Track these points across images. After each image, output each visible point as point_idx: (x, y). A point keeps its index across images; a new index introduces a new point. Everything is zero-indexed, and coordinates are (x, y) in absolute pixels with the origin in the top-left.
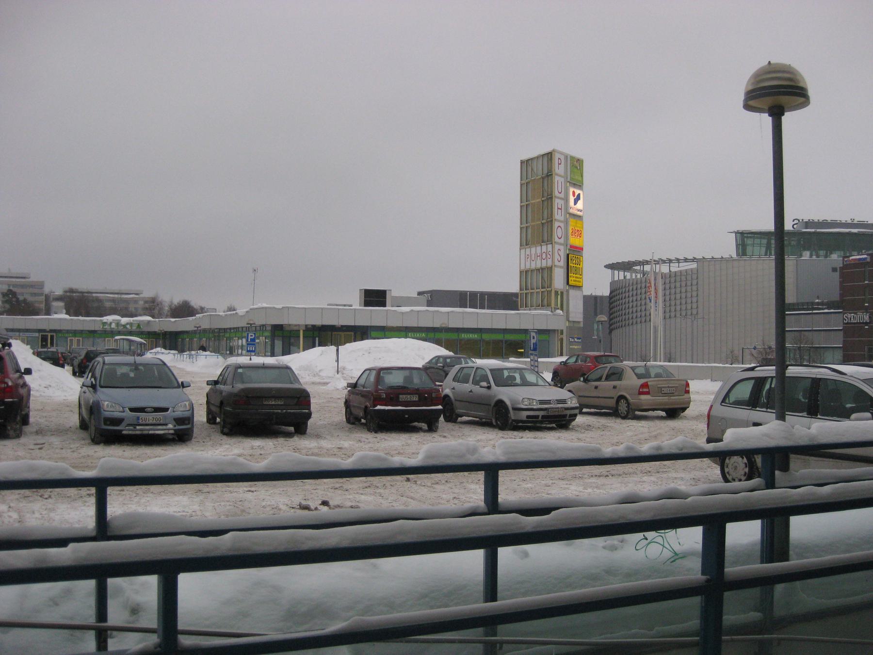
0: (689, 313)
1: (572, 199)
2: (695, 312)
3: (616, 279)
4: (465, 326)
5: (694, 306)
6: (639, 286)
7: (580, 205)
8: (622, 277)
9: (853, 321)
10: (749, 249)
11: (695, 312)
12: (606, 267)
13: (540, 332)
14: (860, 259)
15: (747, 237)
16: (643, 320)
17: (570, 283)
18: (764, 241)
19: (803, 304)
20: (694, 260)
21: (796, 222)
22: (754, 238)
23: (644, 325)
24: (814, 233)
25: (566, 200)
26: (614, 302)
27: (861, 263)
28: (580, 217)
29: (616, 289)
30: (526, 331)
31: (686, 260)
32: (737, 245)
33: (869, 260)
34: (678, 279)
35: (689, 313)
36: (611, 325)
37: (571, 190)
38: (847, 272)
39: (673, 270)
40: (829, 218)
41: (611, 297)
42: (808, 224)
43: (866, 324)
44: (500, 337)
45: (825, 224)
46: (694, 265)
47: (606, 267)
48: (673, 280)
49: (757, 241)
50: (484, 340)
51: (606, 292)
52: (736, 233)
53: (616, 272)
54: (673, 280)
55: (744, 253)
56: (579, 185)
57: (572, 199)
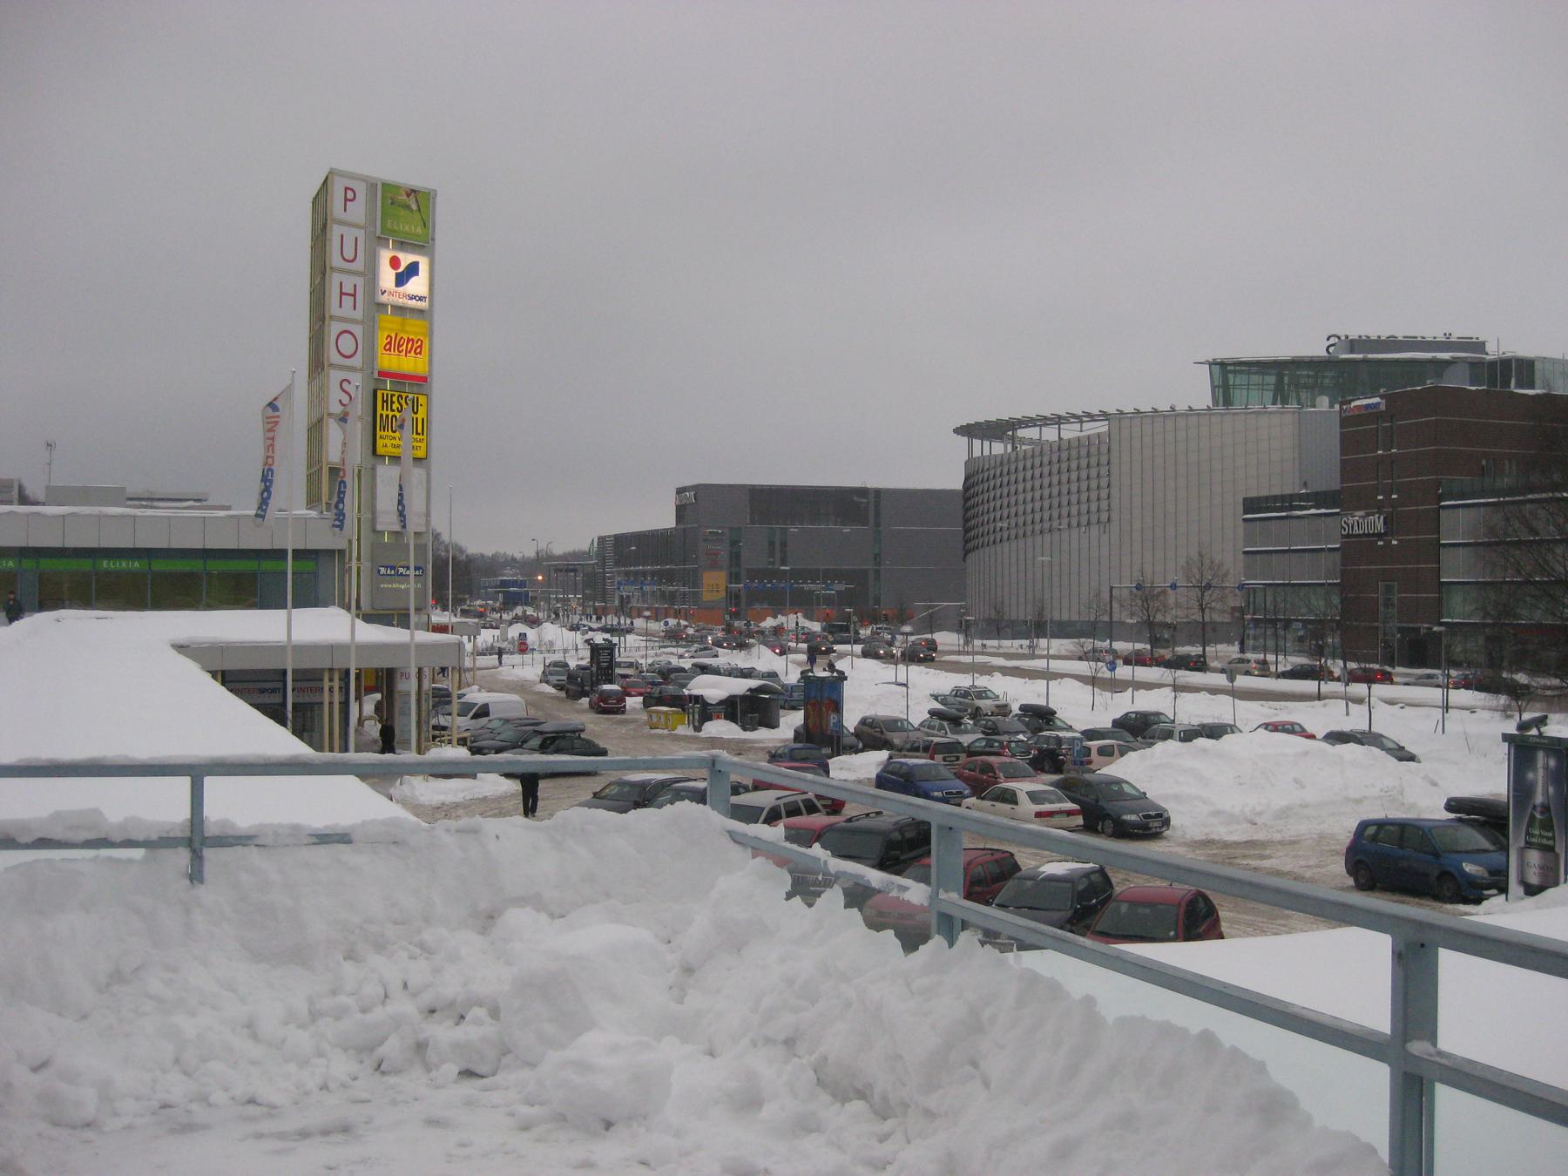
0: (1094, 519)
1: (387, 277)
2: (1104, 517)
3: (977, 453)
4: (176, 545)
5: (1104, 505)
6: (1013, 468)
7: (418, 285)
8: (986, 453)
9: (1356, 531)
10: (1238, 395)
11: (1104, 517)
12: (960, 431)
13: (299, 554)
14: (1368, 406)
15: (1235, 372)
16: (1021, 533)
17: (380, 450)
18: (1271, 379)
19: (1275, 498)
20: (1105, 415)
21: (1333, 340)
22: (1249, 373)
23: (1047, 537)
24: (1364, 361)
25: (371, 274)
26: (971, 502)
27: (1370, 414)
28: (421, 311)
29: (975, 475)
30: (280, 554)
31: (1091, 417)
32: (1213, 387)
33: (1383, 407)
34: (1074, 453)
35: (1094, 519)
36: (966, 542)
37: (385, 256)
38: (1355, 432)
39: (1066, 435)
40: (1400, 334)
41: (967, 486)
42: (1353, 345)
43: (1380, 536)
44: (86, 565)
45: (1392, 344)
46: (1101, 427)
47: (960, 431)
48: (1064, 455)
49: (1255, 379)
50: (209, 575)
51: (958, 484)
52: (1212, 364)
53: (977, 443)
54: (1064, 455)
55: (1228, 402)
56: (423, 245)
57: (387, 277)
